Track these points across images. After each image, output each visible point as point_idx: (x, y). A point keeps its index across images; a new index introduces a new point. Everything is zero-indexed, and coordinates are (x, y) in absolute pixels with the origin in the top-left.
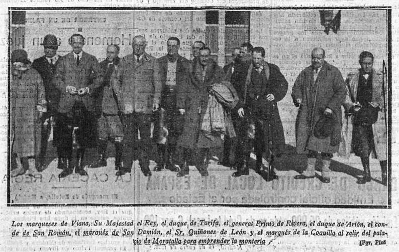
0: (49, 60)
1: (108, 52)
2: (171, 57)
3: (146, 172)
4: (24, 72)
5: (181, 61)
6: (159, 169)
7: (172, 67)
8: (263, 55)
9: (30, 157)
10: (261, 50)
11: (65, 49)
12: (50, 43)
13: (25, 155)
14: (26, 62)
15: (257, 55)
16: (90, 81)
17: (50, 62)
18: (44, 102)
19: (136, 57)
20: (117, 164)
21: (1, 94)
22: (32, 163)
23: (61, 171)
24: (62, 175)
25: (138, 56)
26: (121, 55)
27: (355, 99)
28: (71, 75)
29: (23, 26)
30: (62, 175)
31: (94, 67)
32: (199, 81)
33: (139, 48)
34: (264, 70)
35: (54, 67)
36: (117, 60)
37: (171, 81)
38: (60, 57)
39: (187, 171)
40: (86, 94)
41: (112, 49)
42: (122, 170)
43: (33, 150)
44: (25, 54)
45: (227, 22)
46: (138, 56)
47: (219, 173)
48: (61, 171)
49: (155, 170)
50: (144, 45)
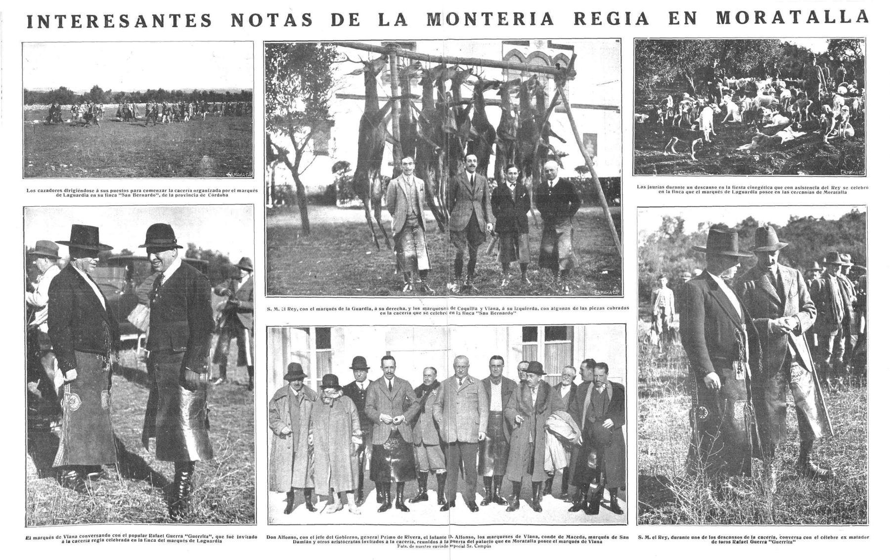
0: (359, 384)
1: (425, 375)
2: (495, 377)
3: (473, 507)
4: (335, 399)
5: (508, 385)
6: (486, 502)
7: (496, 390)
8: (607, 371)
9: (348, 492)
10: (604, 366)
11: (375, 373)
12: (359, 364)
13: (342, 490)
14: (337, 387)
15: (599, 371)
16: (405, 407)
17: (360, 387)
18: (359, 432)
19: (458, 380)
20: (440, 500)
21: (682, 3)
22: (351, 497)
23: (380, 505)
24: (382, 510)
25: (461, 379)
26: (440, 378)
27: (156, 275)
28: (383, 401)
29: (328, 350)
30: (382, 510)
31: (408, 394)
32: (527, 406)
33: (461, 368)
34: (605, 390)
35: (365, 392)
36: (436, 384)
37: (497, 405)
38: (371, 381)
39: (517, 505)
40: (402, 421)
41: (429, 372)
42: (447, 505)
43: (350, 484)
44: (335, 379)
45: (547, 338)
46: (461, 379)
47: (555, 507)
48: (380, 505)
49: (482, 504)
50: (467, 366)
